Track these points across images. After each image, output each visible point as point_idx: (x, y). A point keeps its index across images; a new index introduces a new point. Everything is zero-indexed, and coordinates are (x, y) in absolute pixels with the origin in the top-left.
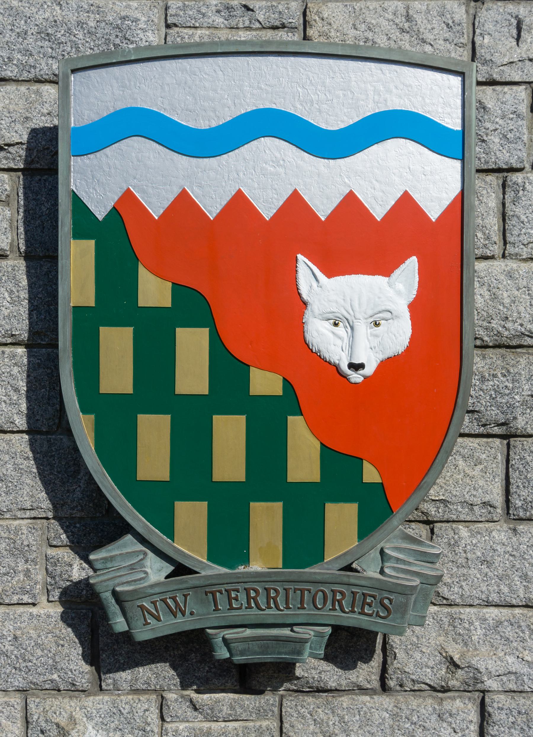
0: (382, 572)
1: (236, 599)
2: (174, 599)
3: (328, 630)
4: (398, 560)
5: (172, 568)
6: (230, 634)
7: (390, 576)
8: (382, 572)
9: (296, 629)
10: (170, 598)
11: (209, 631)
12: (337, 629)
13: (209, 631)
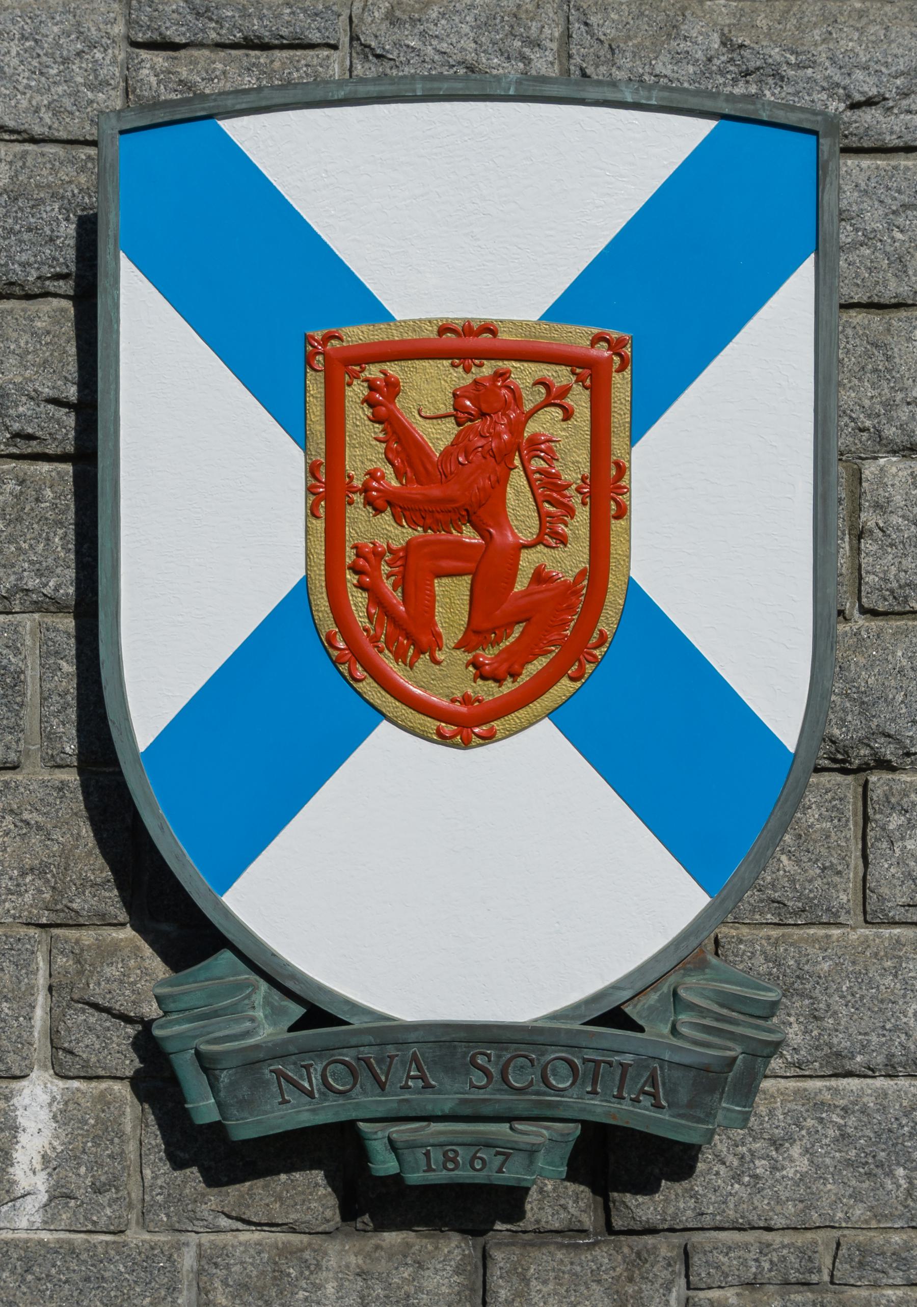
0: (674, 1031)
3: (575, 1130)
5: (298, 1011)
6: (399, 1131)
9: (518, 1126)
11: (361, 1125)
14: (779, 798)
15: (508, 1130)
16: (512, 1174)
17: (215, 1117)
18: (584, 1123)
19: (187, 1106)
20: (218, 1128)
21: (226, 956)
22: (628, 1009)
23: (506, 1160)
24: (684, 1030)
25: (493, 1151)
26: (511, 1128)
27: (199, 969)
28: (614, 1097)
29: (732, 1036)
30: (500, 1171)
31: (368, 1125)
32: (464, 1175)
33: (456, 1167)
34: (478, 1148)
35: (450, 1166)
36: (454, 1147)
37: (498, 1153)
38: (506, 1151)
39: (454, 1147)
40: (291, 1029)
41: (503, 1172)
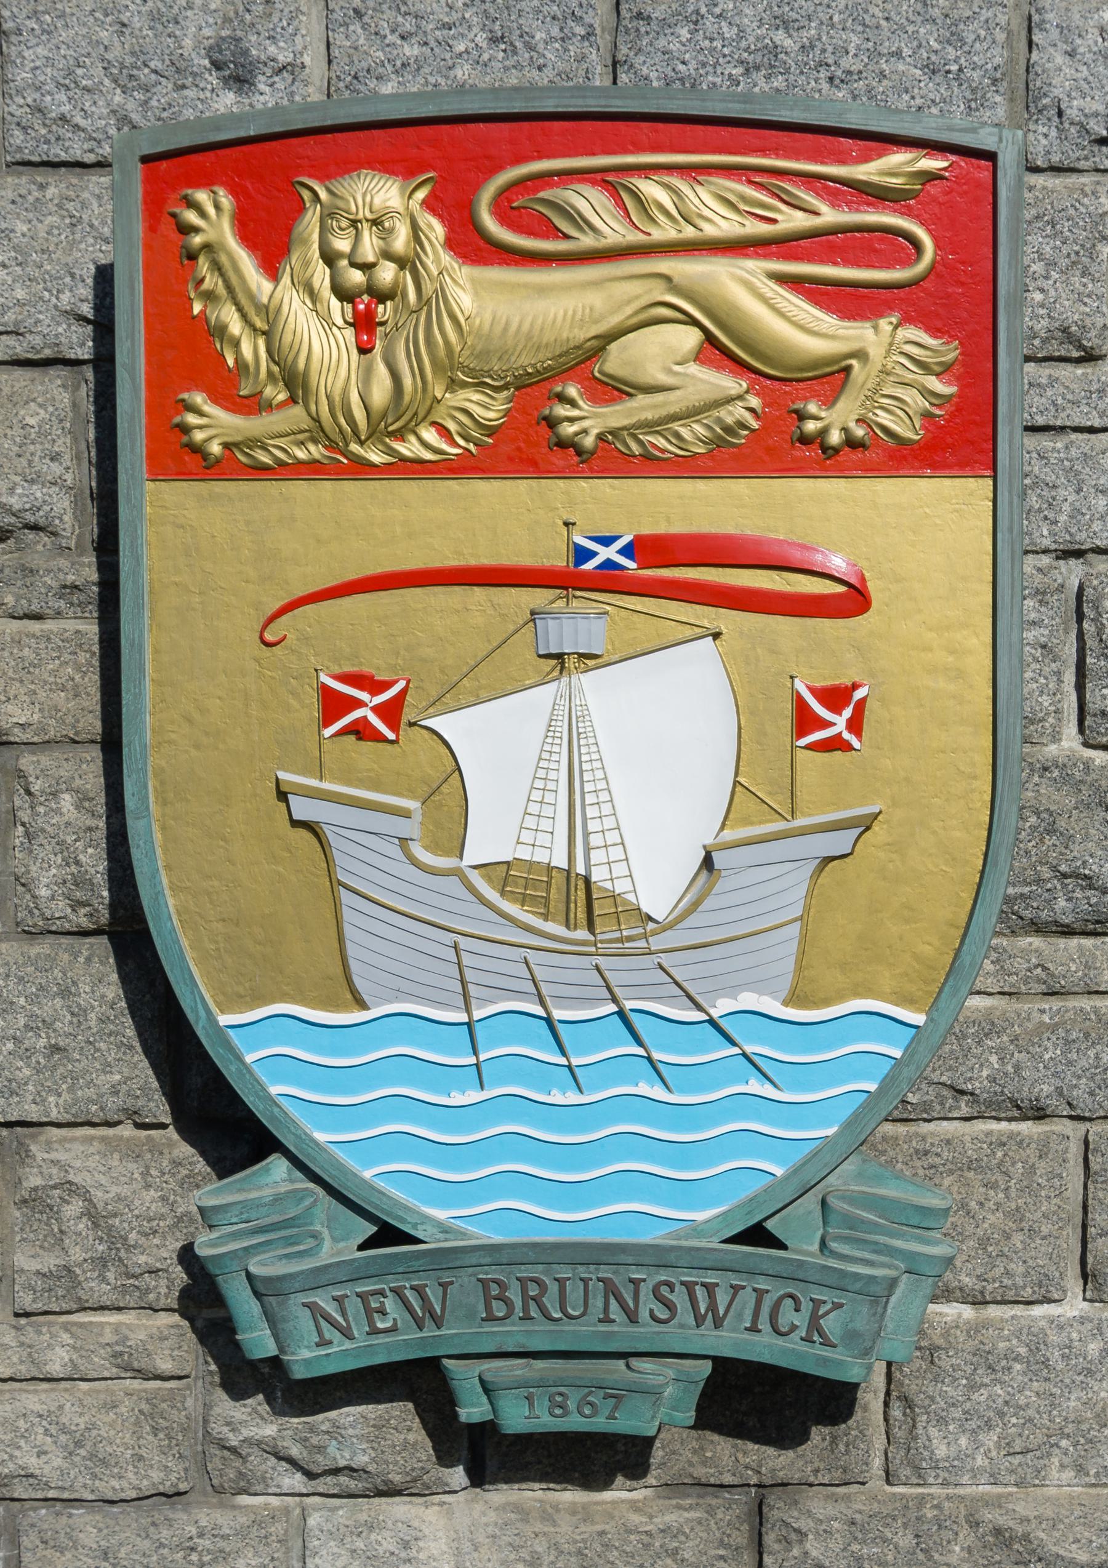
1: (382, 1312)
2: (418, 1290)
3: (706, 1367)
10: (412, 1288)
11: (445, 1361)
12: (720, 1363)
13: (445, 1361)
14: (1013, 584)
15: (624, 1367)
16: (627, 1423)
17: (270, 1349)
18: (715, 1359)
19: (238, 1337)
20: (275, 1362)
22: (769, 1225)
23: (616, 1408)
24: (833, 1245)
25: (601, 1393)
26: (628, 1366)
27: (254, 1174)
28: (802, 1339)
29: (891, 1251)
30: (611, 1417)
31: (453, 1361)
32: (575, 1422)
33: (566, 1413)
34: (587, 1390)
35: (558, 1411)
36: (563, 1389)
37: (607, 1396)
38: (617, 1396)
39: (563, 1389)
40: (362, 1247)
41: (616, 1419)
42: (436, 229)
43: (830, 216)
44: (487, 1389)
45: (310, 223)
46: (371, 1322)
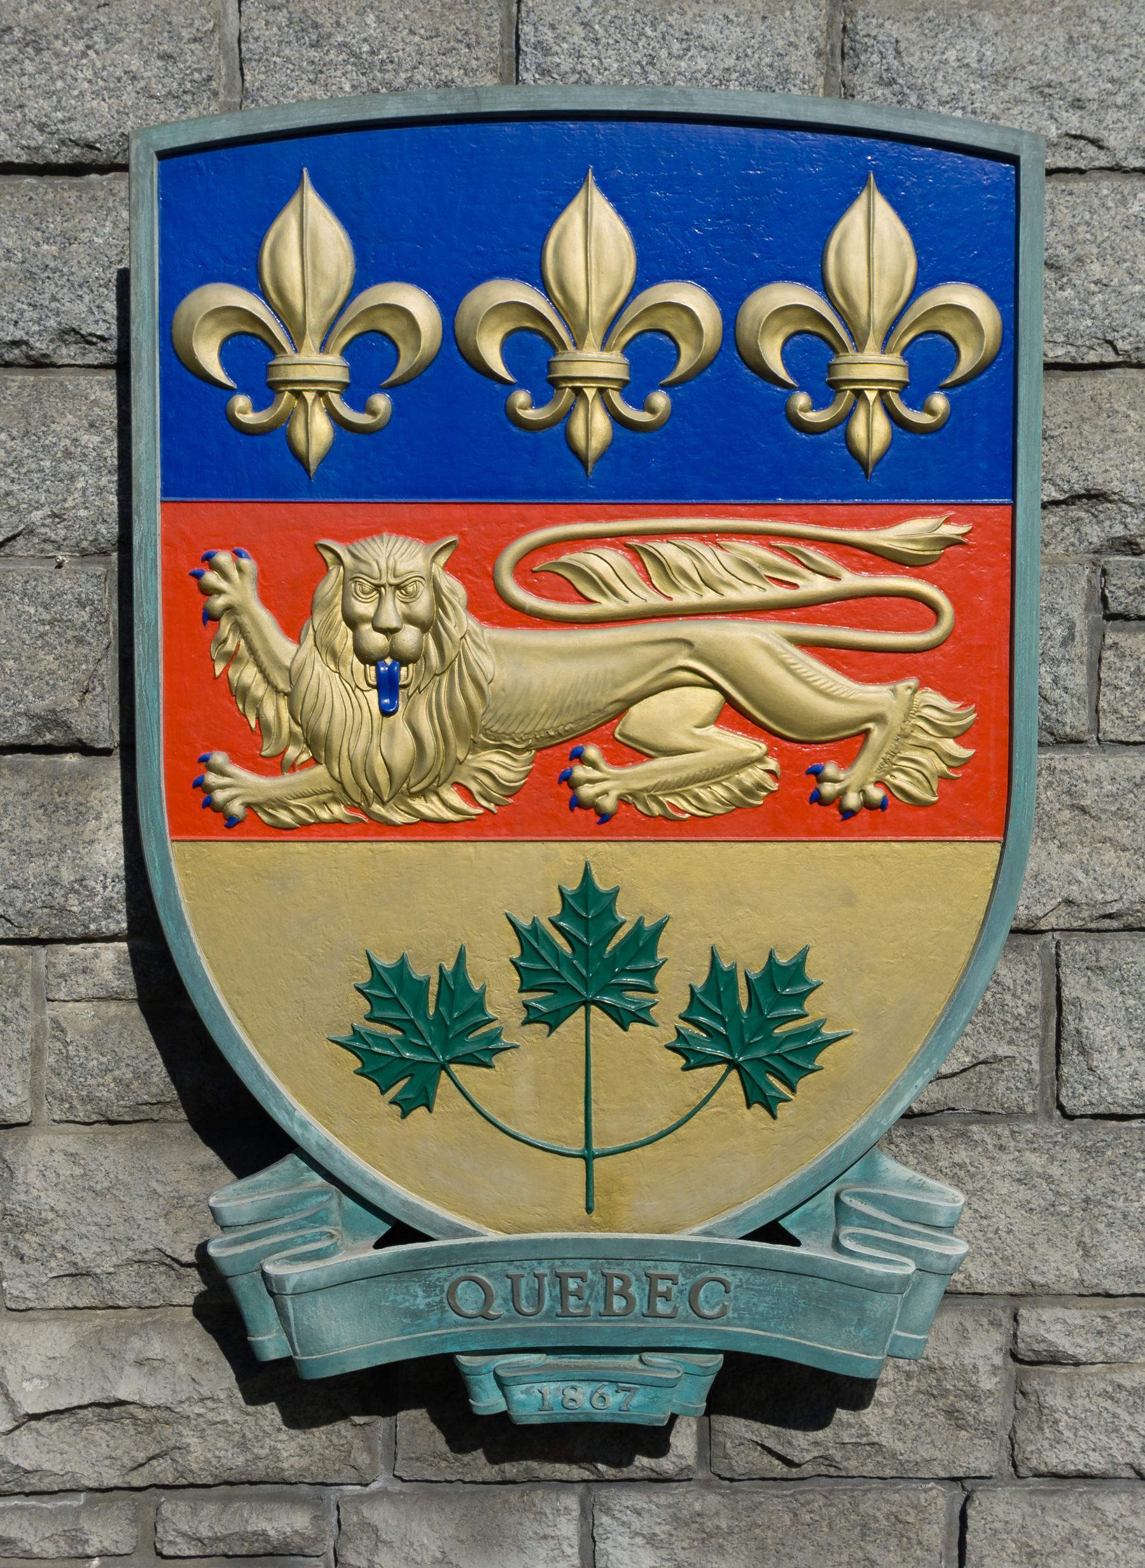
4: (873, 1223)
7: (851, 1254)
8: (837, 1245)
11: (462, 1359)
12: (732, 1358)
21: (290, 1164)
22: (784, 1223)
42: (454, 589)
43: (852, 581)
44: (501, 1383)
45: (330, 585)
46: (651, 1303)
